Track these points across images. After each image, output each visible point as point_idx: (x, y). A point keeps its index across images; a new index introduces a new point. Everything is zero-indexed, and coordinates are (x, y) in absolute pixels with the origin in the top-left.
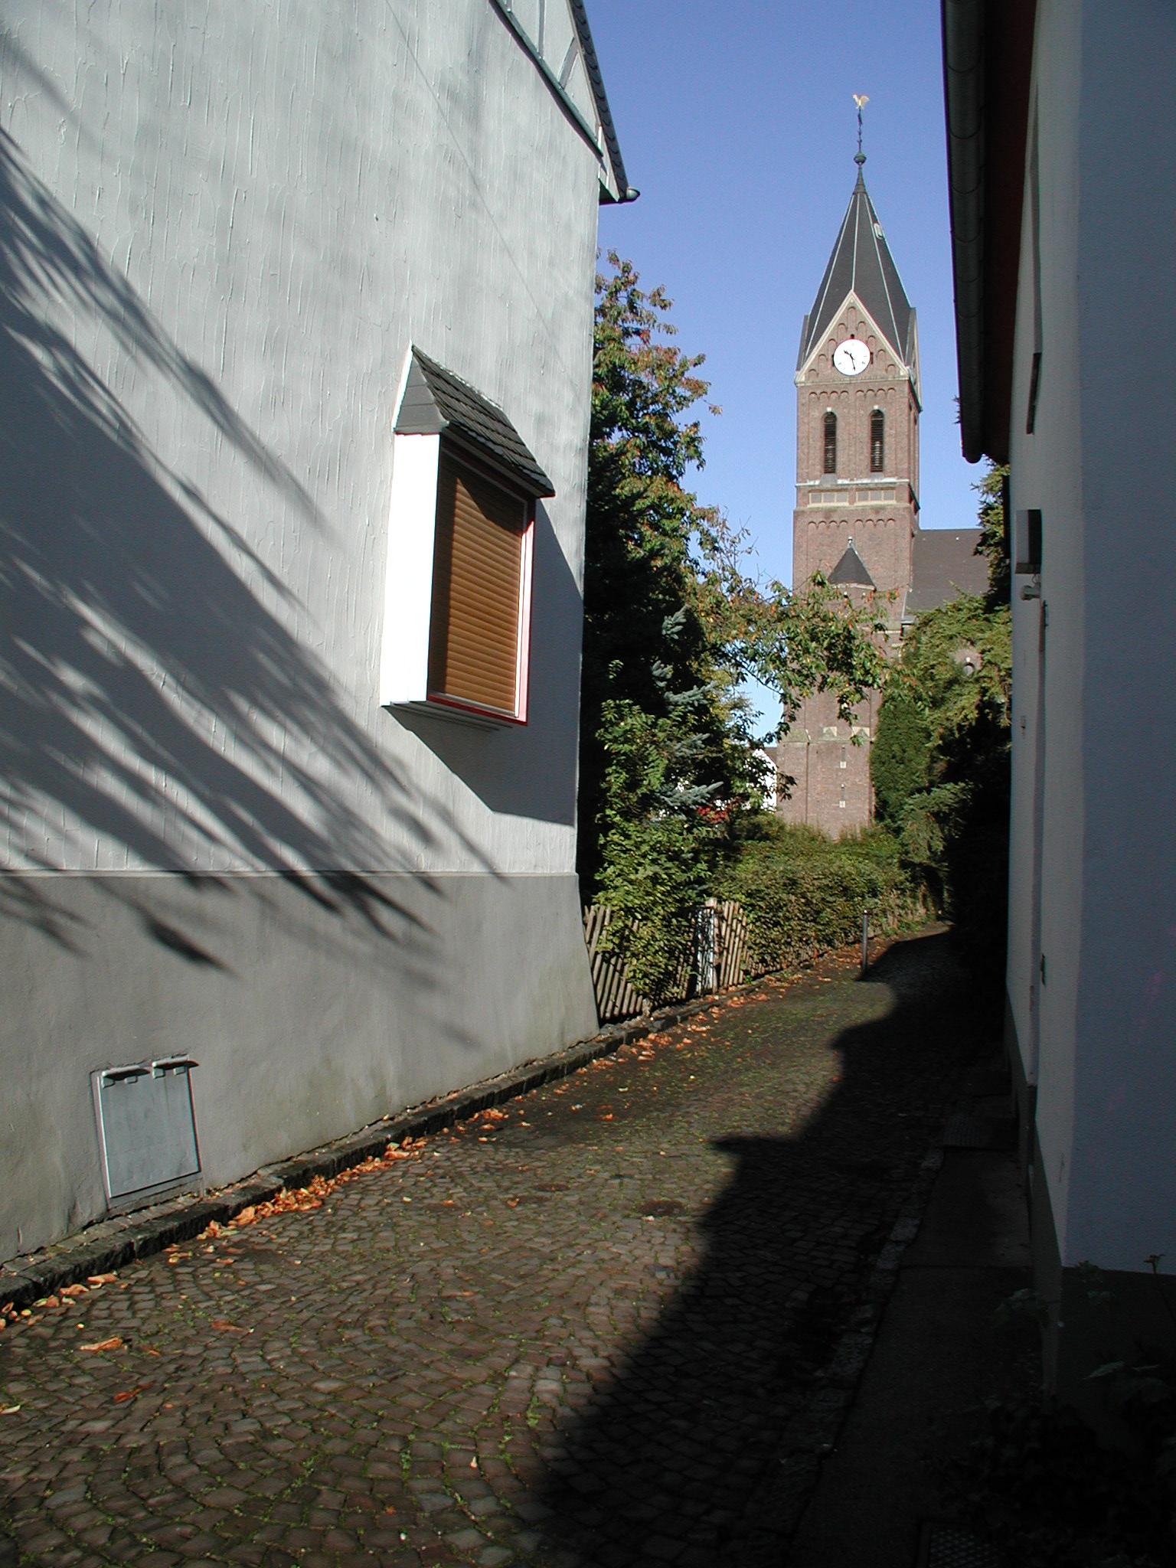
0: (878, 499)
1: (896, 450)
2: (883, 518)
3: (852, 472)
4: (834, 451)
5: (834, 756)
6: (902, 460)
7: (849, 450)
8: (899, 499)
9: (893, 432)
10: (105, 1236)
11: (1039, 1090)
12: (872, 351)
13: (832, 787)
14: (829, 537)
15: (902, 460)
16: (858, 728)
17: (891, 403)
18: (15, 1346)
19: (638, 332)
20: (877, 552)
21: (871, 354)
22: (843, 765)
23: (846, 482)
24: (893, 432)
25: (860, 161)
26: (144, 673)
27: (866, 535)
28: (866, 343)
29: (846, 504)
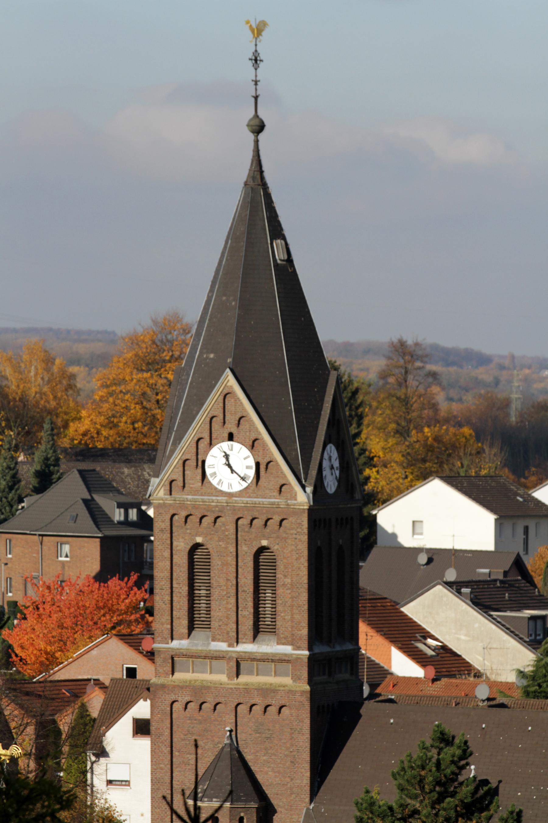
0: (267, 674)
6: (300, 622)
8: (296, 678)
9: (288, 581)
10: (23, 657)
11: (451, 645)
12: (259, 460)
14: (201, 723)
15: (300, 622)
17: (286, 539)
18: (152, 500)
19: (140, 324)
20: (266, 749)
21: (258, 465)
27: (251, 724)
29: (223, 678)
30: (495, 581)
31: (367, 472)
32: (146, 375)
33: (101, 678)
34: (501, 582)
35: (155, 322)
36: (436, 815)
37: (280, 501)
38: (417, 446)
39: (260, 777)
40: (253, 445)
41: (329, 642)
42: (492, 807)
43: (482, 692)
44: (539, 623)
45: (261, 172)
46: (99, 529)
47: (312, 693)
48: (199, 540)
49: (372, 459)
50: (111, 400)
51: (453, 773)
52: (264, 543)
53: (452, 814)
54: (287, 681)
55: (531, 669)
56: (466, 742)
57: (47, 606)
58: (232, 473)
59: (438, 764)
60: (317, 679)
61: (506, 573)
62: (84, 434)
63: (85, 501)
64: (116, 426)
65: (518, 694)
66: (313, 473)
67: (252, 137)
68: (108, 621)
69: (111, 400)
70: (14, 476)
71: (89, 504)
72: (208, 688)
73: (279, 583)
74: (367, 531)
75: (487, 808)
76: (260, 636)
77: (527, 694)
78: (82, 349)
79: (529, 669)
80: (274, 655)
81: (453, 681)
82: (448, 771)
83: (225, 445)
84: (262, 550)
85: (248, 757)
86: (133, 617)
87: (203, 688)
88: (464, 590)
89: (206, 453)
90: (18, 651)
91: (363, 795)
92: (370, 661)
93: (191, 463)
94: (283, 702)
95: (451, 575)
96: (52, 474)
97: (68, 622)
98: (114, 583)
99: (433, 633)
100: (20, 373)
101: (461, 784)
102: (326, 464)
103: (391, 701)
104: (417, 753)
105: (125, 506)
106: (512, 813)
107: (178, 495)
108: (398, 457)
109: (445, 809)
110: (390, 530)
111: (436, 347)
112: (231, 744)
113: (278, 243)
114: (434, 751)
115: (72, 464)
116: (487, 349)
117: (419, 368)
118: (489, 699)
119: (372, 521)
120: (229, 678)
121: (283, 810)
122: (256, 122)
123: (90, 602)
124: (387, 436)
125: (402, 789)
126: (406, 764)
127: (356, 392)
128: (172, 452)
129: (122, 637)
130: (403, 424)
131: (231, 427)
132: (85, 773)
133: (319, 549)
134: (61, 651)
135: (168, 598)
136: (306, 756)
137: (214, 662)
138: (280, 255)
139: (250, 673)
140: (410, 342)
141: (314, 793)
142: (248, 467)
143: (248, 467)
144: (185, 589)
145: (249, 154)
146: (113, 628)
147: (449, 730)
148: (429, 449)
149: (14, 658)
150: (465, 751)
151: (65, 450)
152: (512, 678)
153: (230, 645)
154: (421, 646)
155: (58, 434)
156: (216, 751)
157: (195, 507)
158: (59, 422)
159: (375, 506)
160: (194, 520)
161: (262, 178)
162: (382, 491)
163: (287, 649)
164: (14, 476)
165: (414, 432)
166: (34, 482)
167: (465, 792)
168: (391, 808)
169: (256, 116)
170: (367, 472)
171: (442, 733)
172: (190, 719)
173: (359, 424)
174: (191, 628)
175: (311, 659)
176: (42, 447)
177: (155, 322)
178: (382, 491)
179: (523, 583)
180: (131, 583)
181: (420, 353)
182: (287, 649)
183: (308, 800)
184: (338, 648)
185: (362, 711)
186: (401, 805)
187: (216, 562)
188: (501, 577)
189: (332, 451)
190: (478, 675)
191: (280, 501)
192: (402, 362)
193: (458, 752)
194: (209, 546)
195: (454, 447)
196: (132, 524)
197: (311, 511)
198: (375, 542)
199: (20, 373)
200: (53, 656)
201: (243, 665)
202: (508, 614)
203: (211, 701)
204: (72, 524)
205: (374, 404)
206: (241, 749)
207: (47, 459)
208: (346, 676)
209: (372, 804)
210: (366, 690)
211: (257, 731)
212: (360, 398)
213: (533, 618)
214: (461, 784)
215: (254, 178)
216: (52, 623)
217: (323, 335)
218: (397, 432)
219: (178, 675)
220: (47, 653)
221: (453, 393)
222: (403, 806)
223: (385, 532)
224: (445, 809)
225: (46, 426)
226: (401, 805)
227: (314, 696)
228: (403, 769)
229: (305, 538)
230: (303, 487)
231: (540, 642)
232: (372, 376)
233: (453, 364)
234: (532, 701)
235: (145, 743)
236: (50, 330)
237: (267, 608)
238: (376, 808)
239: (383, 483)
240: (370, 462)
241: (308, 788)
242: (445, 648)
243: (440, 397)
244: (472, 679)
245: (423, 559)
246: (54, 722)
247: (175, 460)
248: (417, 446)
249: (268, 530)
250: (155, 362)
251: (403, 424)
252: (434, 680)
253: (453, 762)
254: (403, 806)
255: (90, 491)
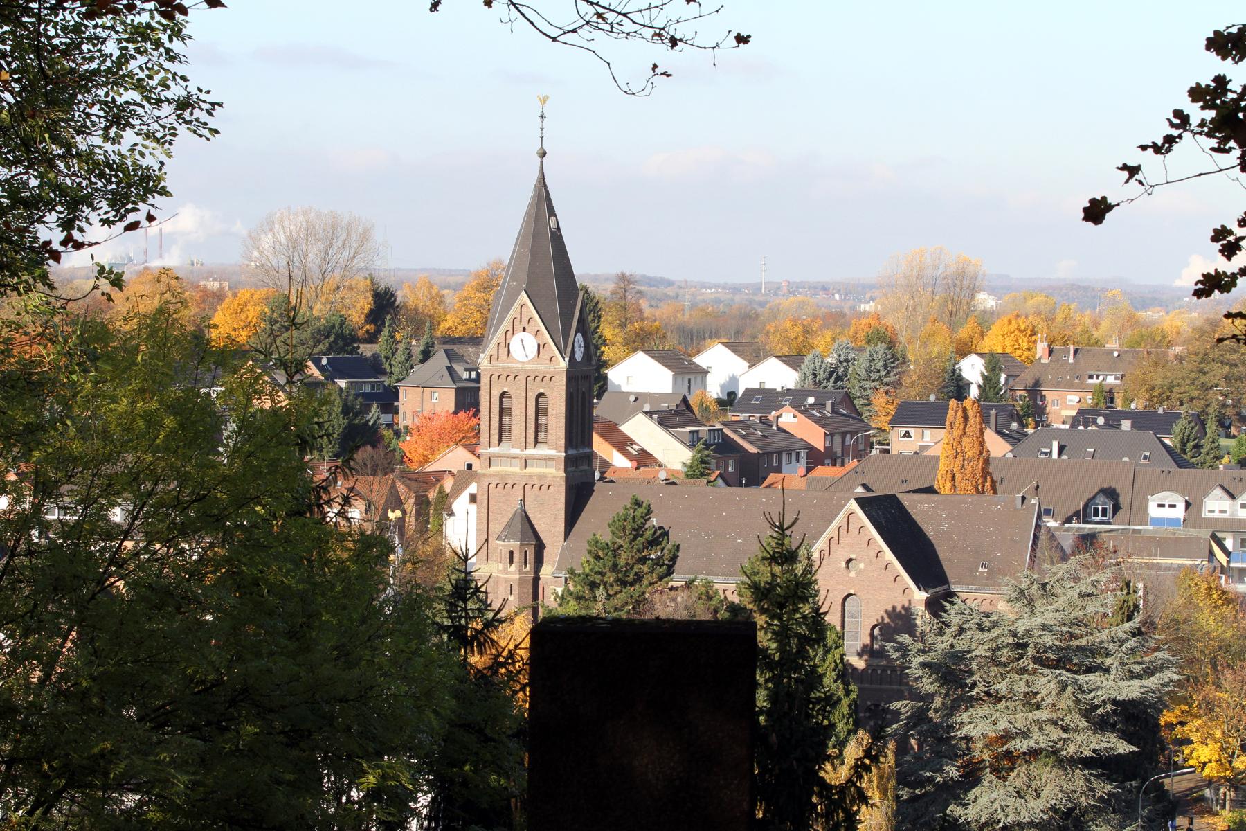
8: (558, 469)
9: (554, 412)
21: (539, 345)
30: (671, 410)
31: (603, 348)
32: (483, 294)
33: (453, 470)
34: (675, 411)
35: (488, 264)
36: (632, 548)
37: (551, 366)
38: (631, 333)
39: (537, 527)
41: (576, 448)
42: (664, 543)
43: (662, 475)
44: (695, 434)
45: (544, 179)
46: (454, 382)
47: (566, 478)
48: (506, 389)
49: (605, 341)
50: (464, 309)
51: (642, 523)
52: (542, 391)
53: (641, 547)
54: (553, 471)
55: (689, 461)
56: (649, 505)
57: (424, 429)
59: (634, 518)
60: (569, 469)
61: (677, 406)
62: (449, 329)
63: (447, 367)
64: (466, 324)
65: (682, 476)
66: (569, 349)
67: (539, 159)
68: (459, 436)
69: (464, 309)
70: (409, 353)
71: (450, 369)
72: (509, 475)
73: (549, 414)
74: (602, 383)
75: (660, 543)
76: (538, 445)
77: (687, 476)
78: (451, 280)
79: (688, 462)
80: (546, 455)
81: (647, 469)
82: (639, 522)
83: (522, 334)
84: (540, 394)
85: (530, 516)
86: (471, 434)
87: (507, 475)
88: (655, 416)
89: (511, 338)
90: (408, 454)
91: (592, 537)
92: (601, 458)
93: (502, 345)
94: (550, 483)
95: (647, 408)
96: (430, 352)
97: (436, 438)
98: (462, 415)
99: (636, 441)
100: (415, 294)
101: (646, 529)
102: (576, 345)
103: (612, 481)
104: (622, 512)
105: (469, 370)
106: (674, 546)
107: (495, 363)
108: (620, 340)
109: (637, 545)
110: (617, 383)
111: (644, 276)
112: (521, 508)
113: (553, 218)
114: (632, 511)
115: (441, 346)
116: (672, 277)
117: (632, 289)
118: (666, 480)
119: (605, 378)
120: (521, 469)
122: (542, 151)
123: (448, 426)
124: (615, 327)
125: (613, 533)
126: (616, 519)
127: (597, 303)
129: (465, 446)
130: (623, 320)
131: (524, 324)
132: (441, 525)
133: (572, 393)
134: (432, 454)
135: (488, 423)
136: (562, 514)
137: (513, 460)
138: (553, 226)
139: (533, 466)
140: (627, 274)
141: (566, 536)
144: (497, 418)
145: (538, 169)
146: (460, 441)
147: (640, 498)
148: (638, 335)
149: (406, 459)
150: (648, 510)
151: (437, 338)
152: (679, 467)
153: (522, 450)
154: (629, 449)
155: (434, 329)
156: (513, 512)
157: (504, 370)
158: (435, 322)
159: (607, 368)
160: (503, 378)
161: (544, 182)
162: (611, 360)
163: (553, 452)
164: (409, 353)
165: (629, 326)
166: (420, 357)
167: (648, 534)
168: (607, 544)
169: (542, 147)
170: (603, 348)
171: (636, 500)
173: (599, 322)
174: (500, 441)
175: (566, 458)
176: (425, 337)
177: (488, 264)
178: (611, 360)
179: (687, 412)
180: (470, 415)
181: (632, 280)
182: (553, 452)
183: (562, 538)
184: (581, 451)
185: (595, 488)
186: (613, 543)
187: (514, 402)
188: (674, 408)
189: (580, 337)
190: (660, 466)
191: (551, 366)
192: (622, 285)
193: (645, 511)
194: (511, 393)
195: (651, 333)
196: (473, 381)
197: (567, 372)
198: (607, 389)
199: (415, 294)
200: (427, 457)
201: (529, 462)
202: (678, 429)
203: (510, 483)
204: (439, 380)
205: (608, 309)
206: (527, 510)
207: (428, 343)
208: (585, 467)
209: (597, 542)
210: (597, 475)
211: (535, 500)
212: (599, 306)
213: (692, 432)
214: (646, 529)
215: (540, 182)
216: (427, 438)
217: (577, 271)
218: (620, 325)
219: (493, 468)
220: (424, 456)
221: (653, 303)
222: (614, 543)
223: (613, 383)
224: (637, 545)
225: (428, 324)
226: (613, 543)
227: (568, 480)
228: (614, 521)
229: (564, 387)
230: (564, 358)
231: (695, 446)
232: (608, 294)
233: (654, 286)
234: (690, 480)
235: (473, 507)
236: (435, 269)
237: (542, 429)
238: (599, 544)
239: (611, 355)
240: (605, 343)
241: (563, 533)
242: (643, 450)
243: (644, 304)
244: (657, 468)
245: (632, 398)
246: (426, 495)
247: (493, 344)
248: (631, 333)
250: (488, 287)
251: (623, 320)
252: (636, 469)
253: (642, 517)
254: (614, 543)
255: (450, 362)
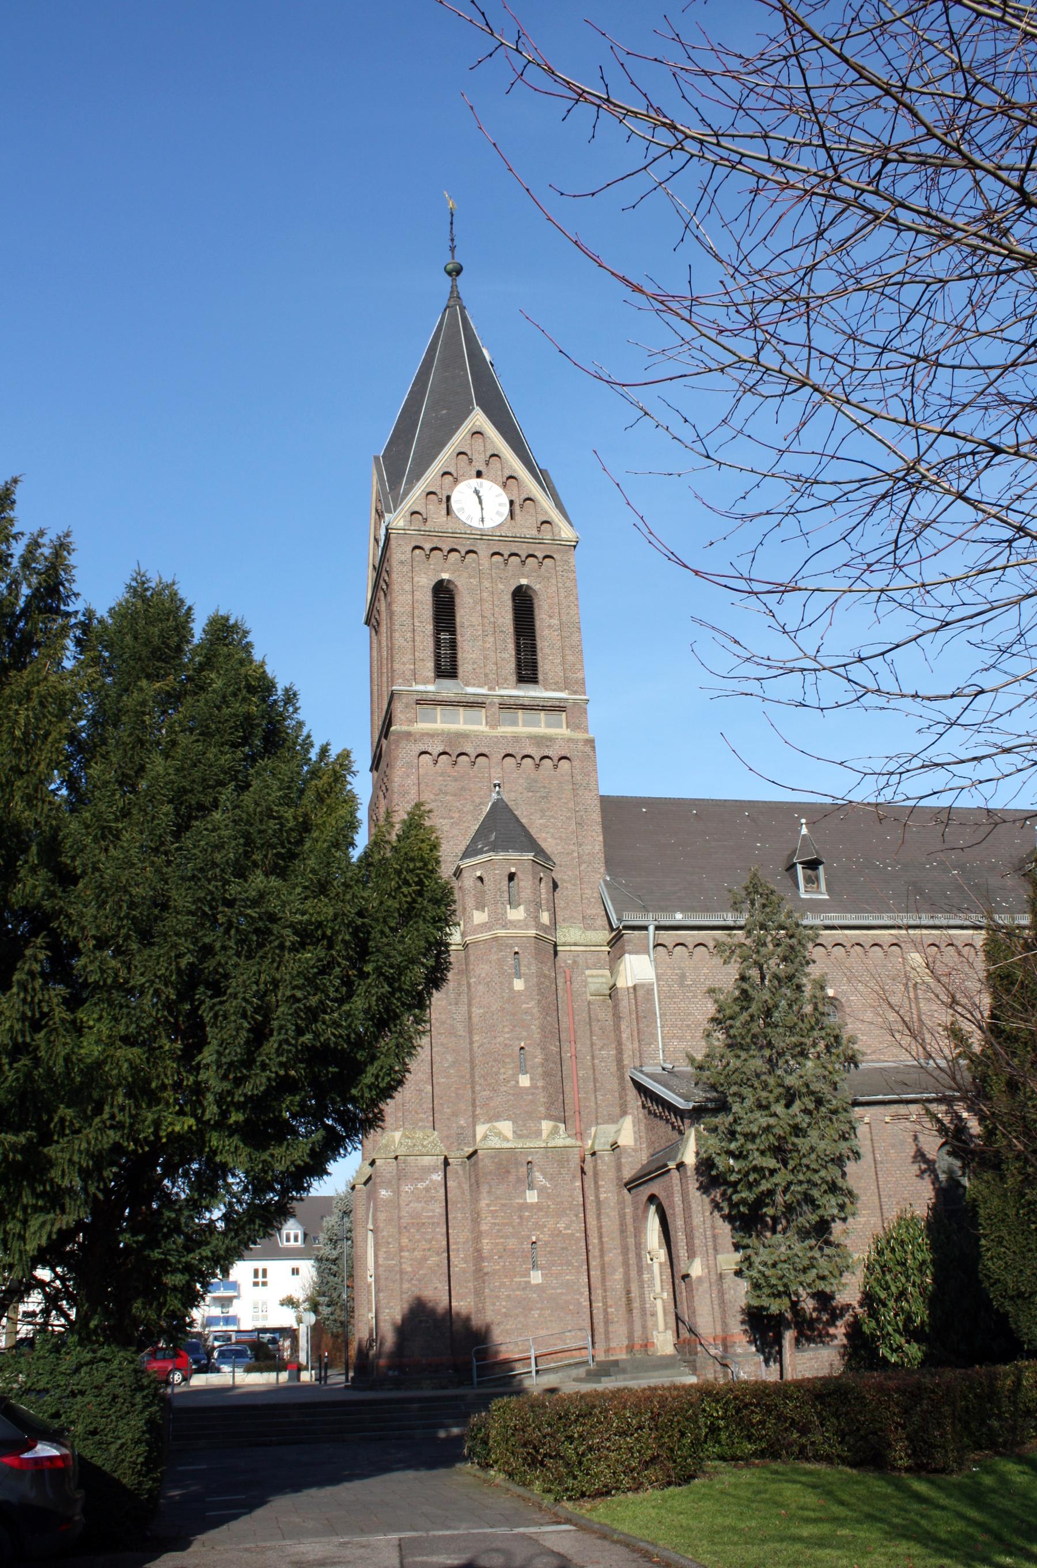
1: (563, 648)
2: (550, 754)
3: (491, 676)
4: (453, 645)
5: (512, 1178)
7: (484, 642)
13: (512, 1243)
16: (487, 1126)
21: (512, 503)
22: (532, 1197)
23: (484, 691)
24: (555, 621)
25: (456, 272)
26: (406, 1311)
28: (504, 486)
40: (510, 480)
58: (368, 622)
83: (475, 482)
121: (569, 886)
128: (407, 493)
142: (500, 505)
143: (500, 505)
172: (442, 774)
249: (526, 569)
